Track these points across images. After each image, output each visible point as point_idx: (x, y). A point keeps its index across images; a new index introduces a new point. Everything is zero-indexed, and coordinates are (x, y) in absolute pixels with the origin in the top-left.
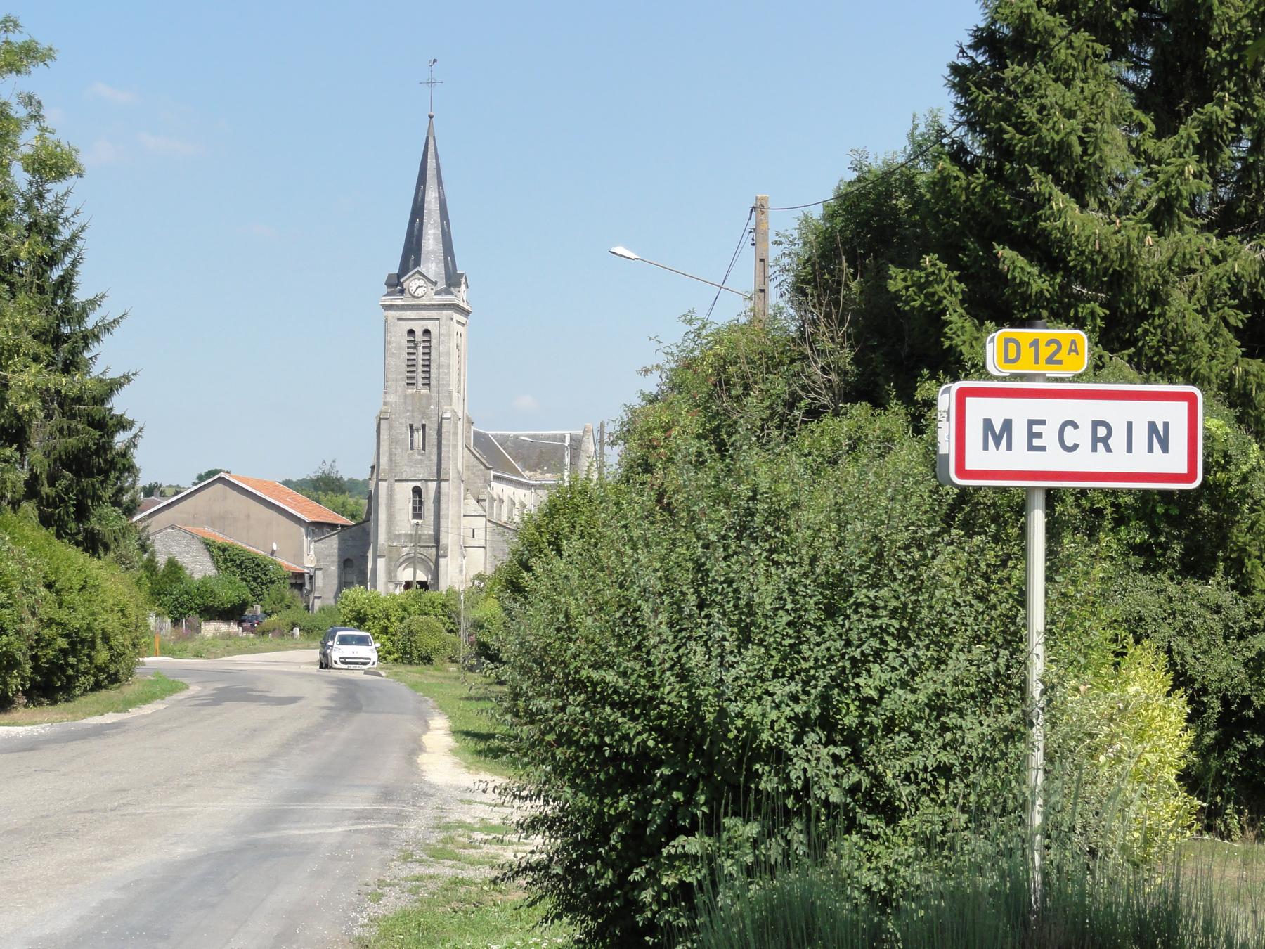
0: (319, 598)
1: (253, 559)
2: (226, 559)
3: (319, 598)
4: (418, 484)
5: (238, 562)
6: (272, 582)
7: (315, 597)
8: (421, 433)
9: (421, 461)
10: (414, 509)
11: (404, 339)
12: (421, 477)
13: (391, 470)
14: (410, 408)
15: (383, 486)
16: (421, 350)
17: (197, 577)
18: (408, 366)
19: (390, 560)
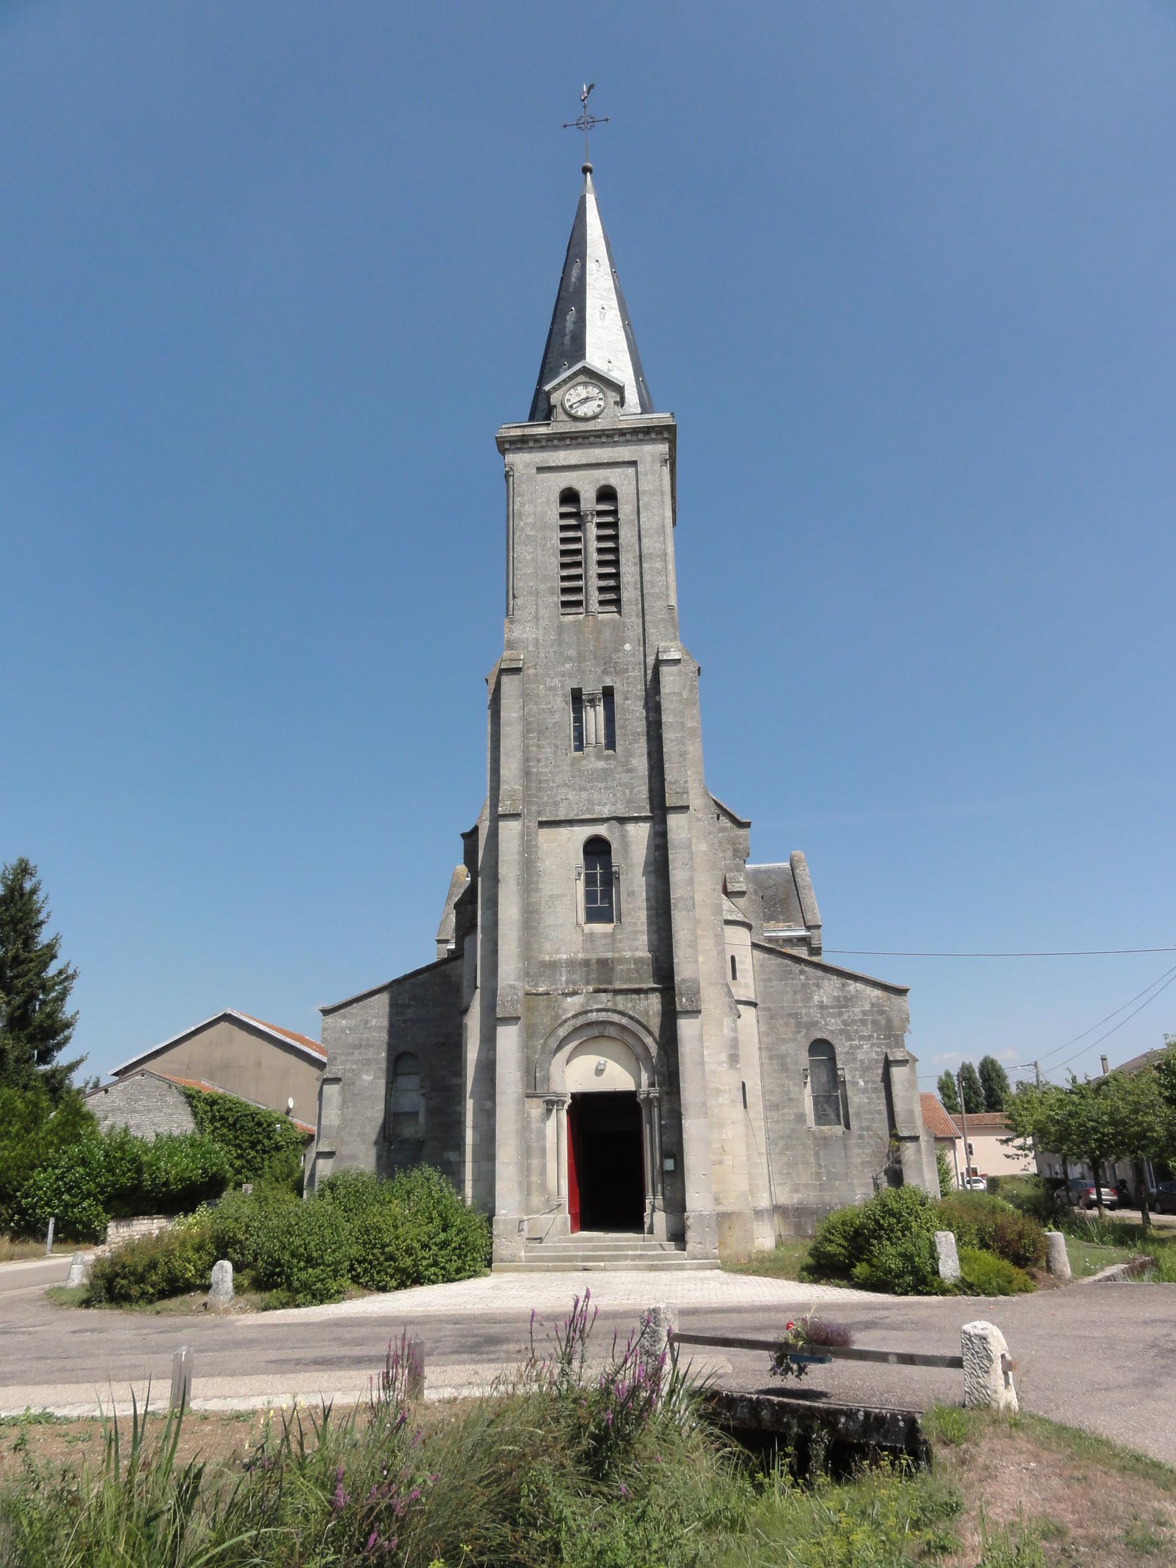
0: (330, 1155)
1: (253, 1115)
2: (214, 1117)
3: (330, 1155)
4: (601, 830)
5: (231, 1120)
6: (278, 1148)
7: (320, 1155)
8: (600, 709)
9: (606, 774)
10: (590, 897)
11: (553, 510)
12: (606, 812)
13: (527, 799)
14: (572, 653)
15: (510, 831)
16: (592, 531)
17: (150, 1138)
18: (564, 566)
19: (529, 1035)
